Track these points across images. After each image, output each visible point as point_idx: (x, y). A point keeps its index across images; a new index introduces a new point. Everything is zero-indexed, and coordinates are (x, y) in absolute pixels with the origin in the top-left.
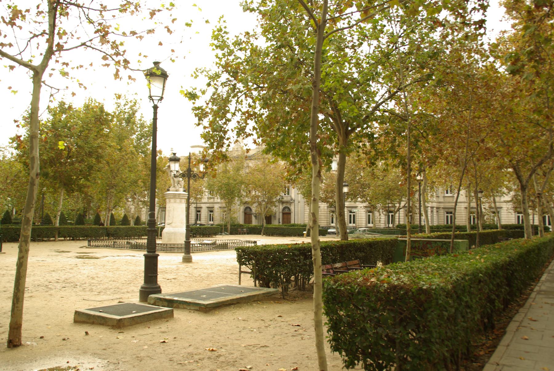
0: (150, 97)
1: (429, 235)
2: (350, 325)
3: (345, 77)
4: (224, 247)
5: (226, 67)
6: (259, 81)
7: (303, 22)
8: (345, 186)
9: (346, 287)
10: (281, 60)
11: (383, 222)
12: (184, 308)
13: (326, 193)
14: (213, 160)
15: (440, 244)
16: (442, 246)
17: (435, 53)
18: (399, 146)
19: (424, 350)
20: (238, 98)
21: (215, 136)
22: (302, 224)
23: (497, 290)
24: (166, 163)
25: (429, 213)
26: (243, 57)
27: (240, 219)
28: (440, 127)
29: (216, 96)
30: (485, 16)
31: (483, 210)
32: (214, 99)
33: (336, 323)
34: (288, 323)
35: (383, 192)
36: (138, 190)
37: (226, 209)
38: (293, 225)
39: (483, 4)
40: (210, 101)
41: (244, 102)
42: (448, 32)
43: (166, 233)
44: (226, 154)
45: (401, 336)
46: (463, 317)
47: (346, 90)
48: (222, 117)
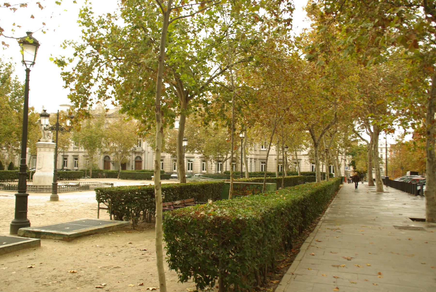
0: (23, 62)
1: (248, 179)
2: (185, 249)
3: (186, 55)
4: (86, 188)
5: (91, 41)
6: (118, 54)
7: (155, 10)
8: (185, 140)
9: (181, 219)
10: (136, 38)
11: (214, 169)
12: (50, 239)
13: (170, 146)
14: (78, 117)
15: (256, 186)
16: (257, 188)
17: (255, 41)
18: (226, 110)
19: (240, 265)
20: (100, 67)
21: (80, 97)
22: (151, 170)
23: (294, 220)
24: (37, 118)
25: (249, 163)
26: (105, 34)
27: (101, 166)
28: (257, 98)
29: (81, 64)
30: (292, 16)
31: (288, 161)
32: (80, 67)
33: (173, 247)
34: (137, 248)
35: (214, 146)
36: (12, 140)
37: (89, 157)
38: (144, 171)
39: (291, 7)
40: (76, 68)
41: (105, 71)
42: (266, 26)
43: (37, 176)
44: (89, 112)
45: (223, 256)
46: (269, 240)
47: (187, 65)
48: (86, 82)
